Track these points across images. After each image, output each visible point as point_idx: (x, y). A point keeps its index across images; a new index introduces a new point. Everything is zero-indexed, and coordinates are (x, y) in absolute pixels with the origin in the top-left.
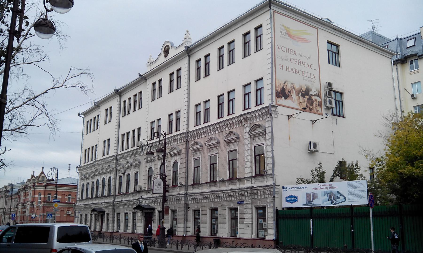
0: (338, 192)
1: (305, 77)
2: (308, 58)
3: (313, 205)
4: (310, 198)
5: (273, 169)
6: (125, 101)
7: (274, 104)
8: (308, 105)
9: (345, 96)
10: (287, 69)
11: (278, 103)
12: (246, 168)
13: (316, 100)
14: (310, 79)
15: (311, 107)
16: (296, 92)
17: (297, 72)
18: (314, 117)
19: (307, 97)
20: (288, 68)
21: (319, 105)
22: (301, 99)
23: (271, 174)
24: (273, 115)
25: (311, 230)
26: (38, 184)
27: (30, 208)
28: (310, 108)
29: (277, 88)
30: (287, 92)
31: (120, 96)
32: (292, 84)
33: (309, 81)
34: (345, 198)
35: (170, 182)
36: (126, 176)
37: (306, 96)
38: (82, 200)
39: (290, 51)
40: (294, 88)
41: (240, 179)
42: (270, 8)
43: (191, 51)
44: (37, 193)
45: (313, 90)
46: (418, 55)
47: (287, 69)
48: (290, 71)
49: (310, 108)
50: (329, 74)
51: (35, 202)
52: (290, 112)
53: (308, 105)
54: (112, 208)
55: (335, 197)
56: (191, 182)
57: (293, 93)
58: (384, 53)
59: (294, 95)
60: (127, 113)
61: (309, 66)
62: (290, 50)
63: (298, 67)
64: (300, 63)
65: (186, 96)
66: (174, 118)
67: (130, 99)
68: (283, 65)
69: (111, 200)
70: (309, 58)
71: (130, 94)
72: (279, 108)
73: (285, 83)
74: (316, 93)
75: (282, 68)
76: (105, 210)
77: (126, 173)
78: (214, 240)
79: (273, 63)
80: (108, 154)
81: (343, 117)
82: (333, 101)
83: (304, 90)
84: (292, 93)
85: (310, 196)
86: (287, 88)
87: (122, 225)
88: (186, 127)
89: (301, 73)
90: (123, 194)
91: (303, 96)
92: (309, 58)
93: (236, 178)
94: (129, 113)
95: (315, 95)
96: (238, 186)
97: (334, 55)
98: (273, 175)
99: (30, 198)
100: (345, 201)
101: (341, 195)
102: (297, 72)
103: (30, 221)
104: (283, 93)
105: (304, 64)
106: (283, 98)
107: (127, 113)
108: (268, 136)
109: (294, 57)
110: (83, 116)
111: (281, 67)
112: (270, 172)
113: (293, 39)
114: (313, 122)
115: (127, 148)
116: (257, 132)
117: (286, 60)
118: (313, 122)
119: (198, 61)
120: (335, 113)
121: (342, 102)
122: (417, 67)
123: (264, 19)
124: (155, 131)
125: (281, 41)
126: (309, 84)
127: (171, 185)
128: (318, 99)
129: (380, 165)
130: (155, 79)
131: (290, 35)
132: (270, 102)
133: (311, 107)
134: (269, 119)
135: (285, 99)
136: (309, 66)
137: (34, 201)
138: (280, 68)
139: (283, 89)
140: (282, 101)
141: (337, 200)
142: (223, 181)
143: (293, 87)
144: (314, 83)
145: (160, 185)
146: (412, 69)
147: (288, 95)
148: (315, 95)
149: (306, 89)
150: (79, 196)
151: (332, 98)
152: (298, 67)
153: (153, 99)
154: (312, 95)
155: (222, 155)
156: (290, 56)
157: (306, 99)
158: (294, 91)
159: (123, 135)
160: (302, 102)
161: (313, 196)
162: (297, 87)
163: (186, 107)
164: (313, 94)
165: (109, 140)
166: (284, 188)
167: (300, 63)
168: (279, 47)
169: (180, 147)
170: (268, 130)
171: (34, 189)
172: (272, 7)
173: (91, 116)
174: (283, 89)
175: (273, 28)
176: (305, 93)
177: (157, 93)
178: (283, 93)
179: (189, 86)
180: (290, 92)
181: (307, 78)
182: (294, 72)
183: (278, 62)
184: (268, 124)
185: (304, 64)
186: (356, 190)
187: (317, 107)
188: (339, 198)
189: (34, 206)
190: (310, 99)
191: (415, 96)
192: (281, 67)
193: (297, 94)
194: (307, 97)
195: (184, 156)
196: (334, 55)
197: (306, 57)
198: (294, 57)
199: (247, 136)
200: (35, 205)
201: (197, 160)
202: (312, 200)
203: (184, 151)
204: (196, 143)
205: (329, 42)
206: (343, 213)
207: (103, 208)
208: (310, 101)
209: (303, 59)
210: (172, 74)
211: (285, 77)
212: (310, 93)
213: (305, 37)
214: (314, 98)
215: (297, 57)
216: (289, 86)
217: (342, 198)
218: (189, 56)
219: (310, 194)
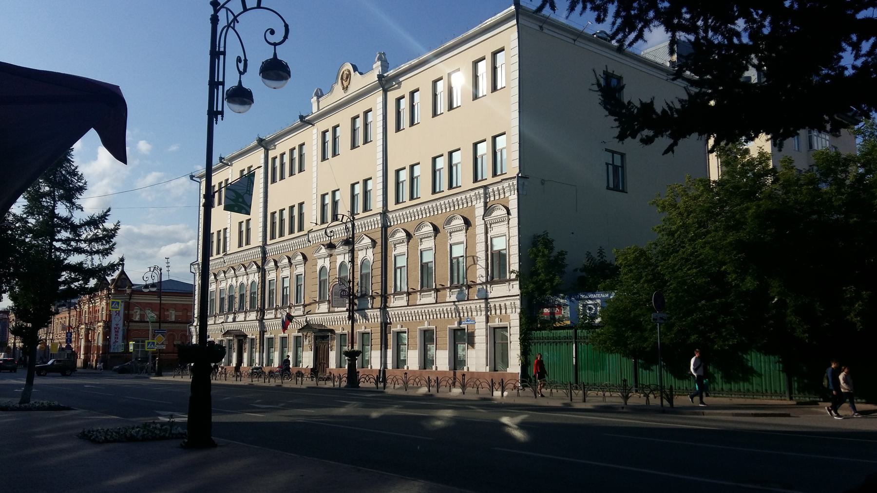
6: (274, 159)
9: (628, 158)
31: (267, 151)
60: (222, 233)
66: (359, 189)
67: (282, 155)
80: (248, 243)
81: (623, 191)
94: (282, 178)
103: (128, 330)
107: (222, 233)
115: (281, 235)
120: (611, 186)
121: (622, 167)
124: (329, 209)
129: (136, 359)
130: (326, 124)
153: (324, 158)
159: (273, 214)
177: (329, 148)
210: (354, 119)
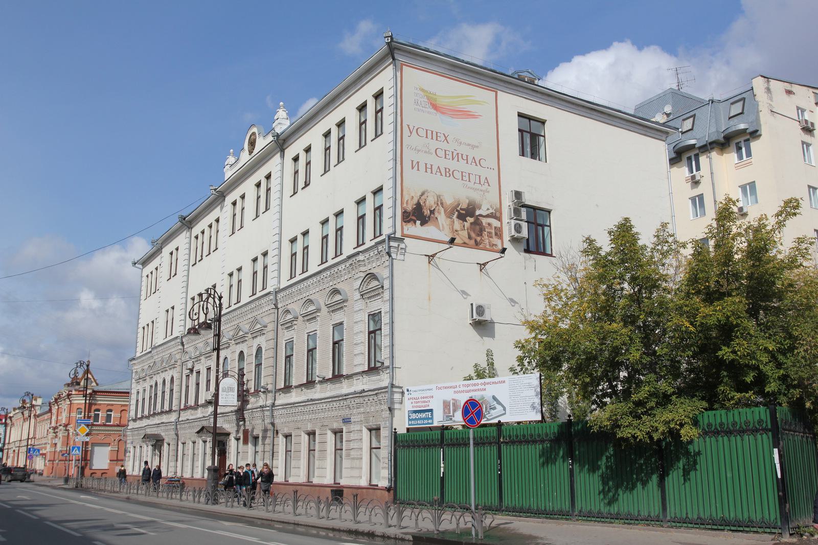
0: (494, 398)
1: (467, 183)
2: (473, 147)
3: (488, 420)
4: (449, 409)
5: (392, 357)
7: (398, 235)
8: (473, 235)
10: (429, 168)
11: (406, 232)
12: (355, 357)
13: (489, 224)
14: (478, 186)
15: (479, 239)
16: (445, 211)
17: (449, 173)
18: (483, 256)
19: (470, 220)
20: (429, 166)
21: (496, 234)
22: (457, 224)
23: (388, 367)
24: (394, 256)
25: (442, 470)
26: (77, 393)
27: (63, 436)
28: (476, 241)
29: (405, 205)
30: (427, 212)
32: (439, 197)
33: (476, 189)
34: (505, 409)
35: (251, 386)
36: (194, 373)
37: (468, 218)
38: (135, 420)
39: (435, 136)
40: (442, 204)
41: (349, 377)
42: (394, 59)
43: (285, 141)
44: (75, 408)
45: (484, 207)
46: (748, 131)
47: (429, 168)
48: (434, 172)
49: (476, 241)
50: (523, 177)
51: (71, 426)
52: (432, 248)
53: (473, 235)
54: (174, 433)
55: (488, 406)
56: (281, 385)
57: (439, 213)
58: (648, 130)
59: (442, 217)
61: (477, 162)
62: (434, 134)
63: (452, 165)
64: (456, 156)
65: (277, 223)
68: (418, 163)
69: (173, 417)
70: (477, 147)
71: (203, 224)
72: (407, 240)
73: (423, 194)
74: (491, 211)
75: (416, 168)
76: (164, 437)
77: (194, 370)
78: (332, 491)
79: (398, 158)
82: (525, 226)
83: (464, 206)
84: (436, 214)
85: (449, 406)
86: (427, 203)
87: (188, 464)
88: (275, 281)
89: (456, 174)
90: (191, 408)
91: (462, 217)
92: (477, 147)
93: (342, 376)
95: (487, 216)
96: (345, 388)
97: (531, 139)
98: (392, 368)
99: (63, 419)
100: (505, 414)
101: (499, 403)
102: (449, 173)
104: (417, 214)
105: (465, 157)
106: (418, 222)
108: (387, 295)
109: (444, 145)
110: (141, 266)
111: (415, 165)
112: (387, 363)
113: (443, 113)
114: (482, 266)
116: (372, 285)
117: (426, 152)
118: (482, 266)
119: (296, 159)
122: (749, 154)
123: (384, 79)
125: (410, 118)
126: (476, 196)
127: (252, 391)
128: (495, 223)
131: (435, 107)
132: (390, 231)
133: (479, 239)
134: (387, 263)
135: (422, 224)
136: (477, 162)
137: (69, 424)
138: (413, 168)
139: (418, 208)
140: (416, 229)
141: (492, 412)
142: (324, 381)
143: (440, 202)
144: (486, 194)
145: (231, 389)
146: (740, 157)
147: (429, 217)
148: (487, 216)
149: (469, 205)
150: (132, 414)
151: (521, 220)
152: (452, 165)
154: (481, 215)
155: (324, 330)
156: (434, 144)
157: (467, 225)
158: (442, 210)
160: (458, 229)
161: (454, 404)
162: (449, 201)
163: (276, 245)
164: (484, 214)
165: (173, 308)
166: (408, 390)
167: (456, 156)
168: (411, 128)
169: (266, 320)
170: (387, 284)
171: (70, 401)
172: (396, 56)
173: (151, 267)
174: (418, 208)
175: (399, 96)
176: (467, 213)
178: (417, 214)
179: (281, 205)
180: (432, 212)
181: (471, 184)
182: (443, 173)
183: (408, 156)
184: (385, 273)
185: (465, 157)
186: (522, 395)
187: (491, 237)
188: (494, 408)
189: (69, 434)
190: (477, 223)
191: (745, 211)
192: (415, 165)
193: (449, 215)
194: (470, 220)
195: (271, 335)
196: (531, 139)
197: (469, 145)
198: (444, 145)
199: (357, 295)
200: (71, 431)
201: (290, 344)
202: (451, 414)
203: (271, 327)
204: (288, 311)
205: (521, 115)
206: (487, 438)
207: (163, 434)
208: (478, 227)
209: (463, 150)
211: (418, 184)
212: (478, 213)
213: (468, 108)
214: (485, 221)
215: (450, 147)
216: (430, 202)
217: (499, 408)
218: (282, 151)
219: (449, 403)
